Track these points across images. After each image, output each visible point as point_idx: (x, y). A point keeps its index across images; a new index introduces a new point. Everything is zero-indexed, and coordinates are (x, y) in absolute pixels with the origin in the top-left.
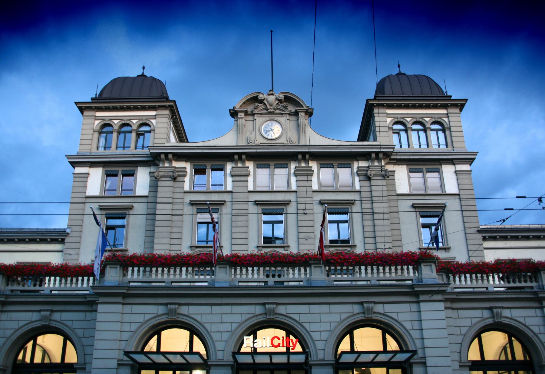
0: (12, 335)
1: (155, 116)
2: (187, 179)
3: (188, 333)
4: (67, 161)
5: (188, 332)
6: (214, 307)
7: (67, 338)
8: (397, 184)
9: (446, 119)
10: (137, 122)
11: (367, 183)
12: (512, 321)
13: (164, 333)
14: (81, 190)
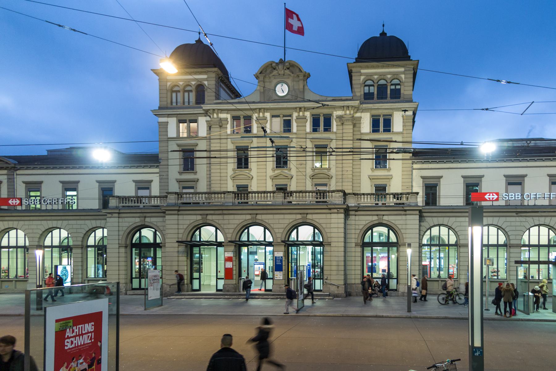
0: (127, 229)
1: (206, 79)
2: (229, 126)
3: (263, 228)
4: (152, 113)
5: (263, 228)
6: (507, 218)
7: (265, 228)
8: (361, 127)
10: (195, 84)
11: (341, 127)
12: (388, 222)
13: (250, 228)
14: (164, 133)
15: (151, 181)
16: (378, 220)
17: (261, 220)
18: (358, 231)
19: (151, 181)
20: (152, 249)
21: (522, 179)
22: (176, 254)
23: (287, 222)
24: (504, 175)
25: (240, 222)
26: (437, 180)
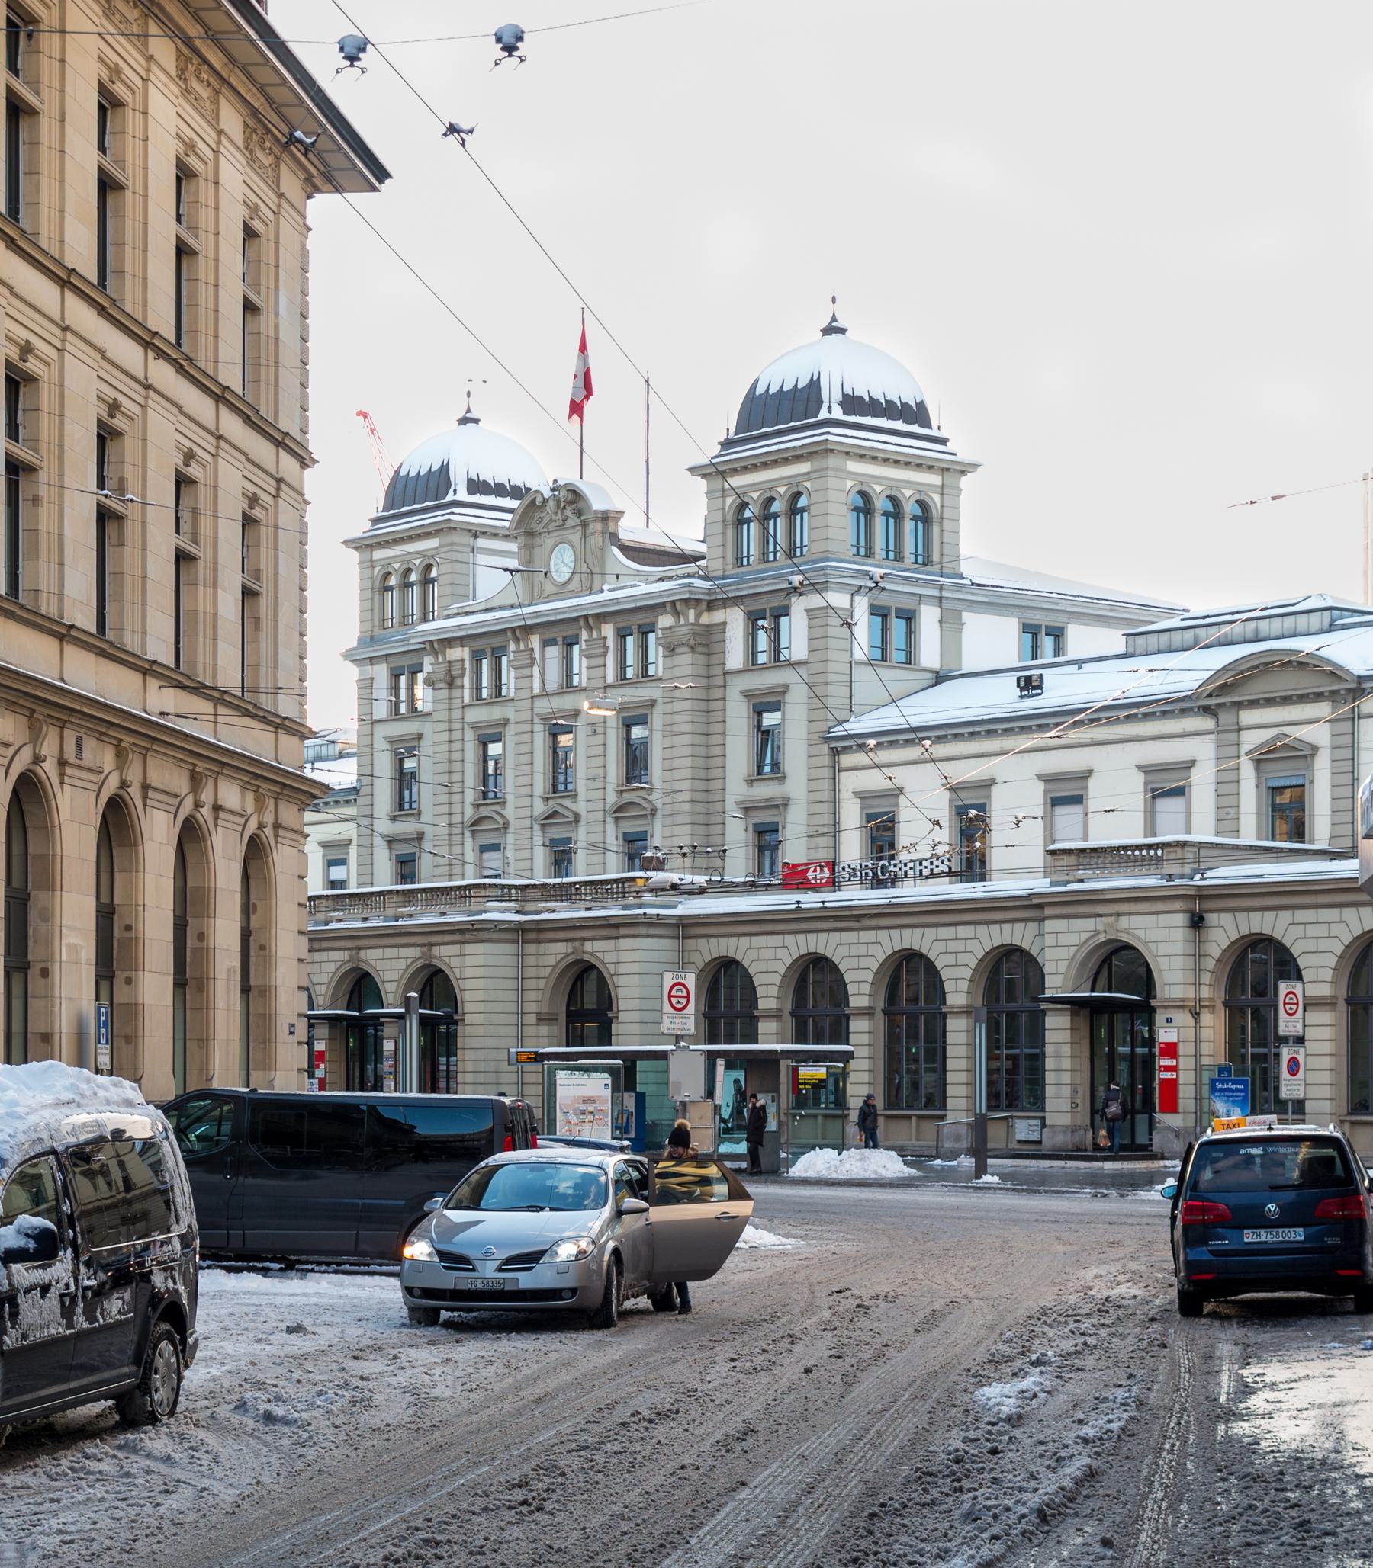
9: (937, 498)
15: (1188, 765)
16: (573, 953)
17: (591, 954)
18: (542, 983)
19: (1188, 765)
20: (1106, 1016)
21: (892, 800)
22: (1310, 1034)
23: (1075, 939)
24: (1139, 767)
25: (1082, 940)
26: (983, 792)
